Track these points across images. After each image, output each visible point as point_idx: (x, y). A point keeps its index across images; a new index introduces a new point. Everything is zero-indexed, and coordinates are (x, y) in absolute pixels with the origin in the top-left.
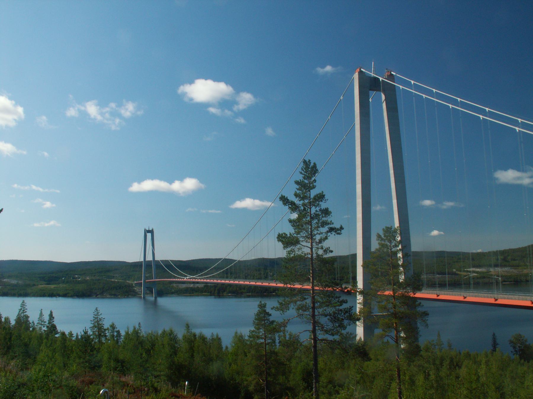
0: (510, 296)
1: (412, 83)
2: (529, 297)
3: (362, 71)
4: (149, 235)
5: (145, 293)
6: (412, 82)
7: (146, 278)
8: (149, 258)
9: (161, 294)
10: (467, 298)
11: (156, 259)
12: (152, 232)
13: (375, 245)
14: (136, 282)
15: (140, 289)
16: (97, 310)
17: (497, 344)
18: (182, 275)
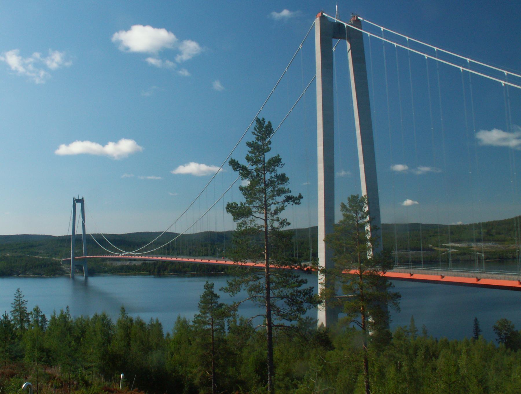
0: (495, 276)
1: (382, 30)
2: (516, 277)
3: (324, 16)
4: (79, 205)
5: (74, 272)
6: (382, 28)
7: (75, 254)
8: (79, 231)
9: (92, 273)
10: (445, 277)
11: (86, 233)
12: (82, 201)
13: (339, 217)
14: (63, 259)
15: (68, 267)
16: (19, 292)
17: (480, 331)
18: (116, 251)
